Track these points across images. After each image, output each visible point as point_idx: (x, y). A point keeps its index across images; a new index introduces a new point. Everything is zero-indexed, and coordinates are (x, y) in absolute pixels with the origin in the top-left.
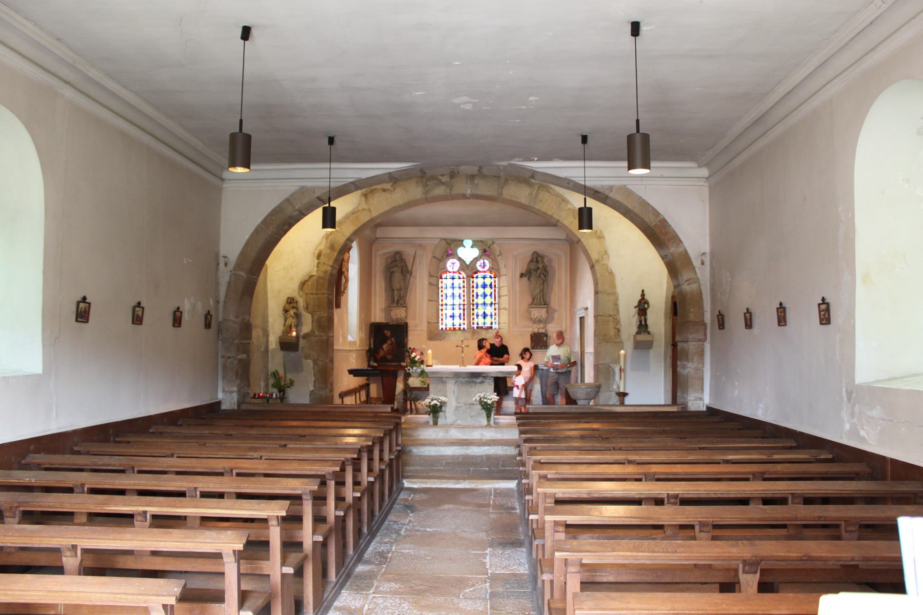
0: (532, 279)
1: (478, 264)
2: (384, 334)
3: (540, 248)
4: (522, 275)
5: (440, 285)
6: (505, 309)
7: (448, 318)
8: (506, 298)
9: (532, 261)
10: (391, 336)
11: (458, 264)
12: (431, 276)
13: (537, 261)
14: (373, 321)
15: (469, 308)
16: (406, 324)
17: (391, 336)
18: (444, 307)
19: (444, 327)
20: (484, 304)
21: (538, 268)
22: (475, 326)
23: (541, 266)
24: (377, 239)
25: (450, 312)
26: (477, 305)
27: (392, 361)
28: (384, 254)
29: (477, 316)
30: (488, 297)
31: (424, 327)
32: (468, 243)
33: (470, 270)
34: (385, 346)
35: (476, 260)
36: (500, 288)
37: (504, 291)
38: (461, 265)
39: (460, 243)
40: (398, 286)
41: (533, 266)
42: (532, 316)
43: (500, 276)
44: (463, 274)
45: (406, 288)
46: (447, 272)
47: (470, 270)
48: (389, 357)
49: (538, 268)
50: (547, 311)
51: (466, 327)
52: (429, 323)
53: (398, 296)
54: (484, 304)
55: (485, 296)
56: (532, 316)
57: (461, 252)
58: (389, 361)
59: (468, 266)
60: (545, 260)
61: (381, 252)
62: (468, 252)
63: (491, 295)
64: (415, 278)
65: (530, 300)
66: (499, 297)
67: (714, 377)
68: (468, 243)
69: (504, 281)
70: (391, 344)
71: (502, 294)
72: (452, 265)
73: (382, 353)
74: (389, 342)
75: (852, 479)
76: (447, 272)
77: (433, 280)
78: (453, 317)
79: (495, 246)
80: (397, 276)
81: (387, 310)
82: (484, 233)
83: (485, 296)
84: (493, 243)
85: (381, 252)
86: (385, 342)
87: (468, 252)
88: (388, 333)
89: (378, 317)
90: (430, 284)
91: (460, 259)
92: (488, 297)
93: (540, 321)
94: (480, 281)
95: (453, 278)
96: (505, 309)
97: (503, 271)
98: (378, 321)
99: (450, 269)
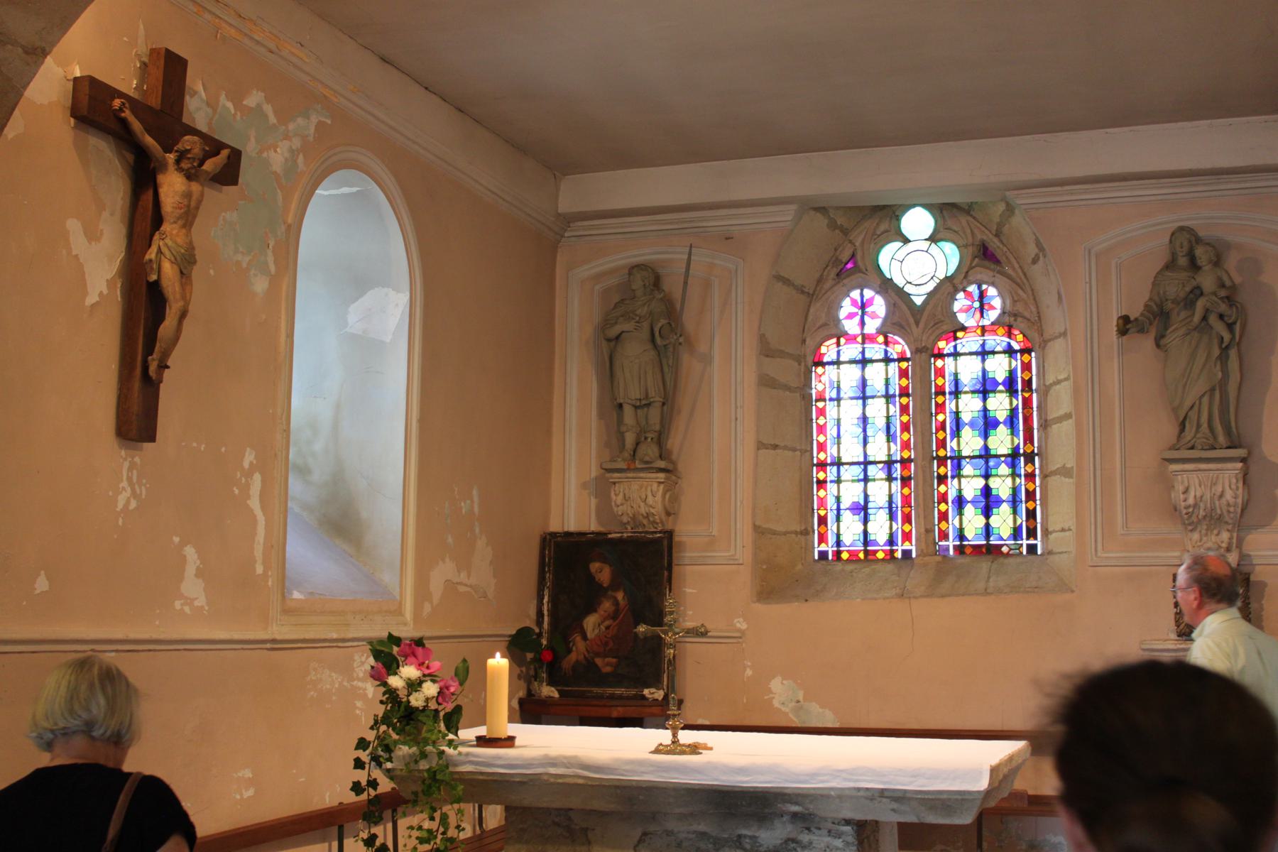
0: (1173, 338)
1: (960, 302)
2: (591, 578)
3: (1209, 214)
4: (1125, 326)
5: (816, 387)
6: (1065, 472)
7: (847, 516)
8: (1068, 426)
9: (1170, 265)
10: (615, 586)
11: (879, 306)
12: (767, 350)
13: (1194, 266)
14: (555, 527)
15: (923, 466)
16: (670, 534)
17: (615, 586)
18: (832, 472)
19: (829, 548)
20: (986, 455)
21: (1197, 292)
22: (951, 543)
23: (1207, 281)
24: (569, 220)
25: (851, 493)
26: (958, 460)
27: (616, 679)
28: (599, 277)
29: (960, 502)
30: (1002, 431)
31: (741, 546)
32: (918, 222)
33: (923, 326)
34: (591, 623)
35: (949, 287)
36: (1045, 391)
37: (1062, 400)
38: (892, 308)
39: (883, 219)
40: (635, 393)
41: (1175, 288)
42: (1177, 496)
43: (1044, 343)
44: (900, 346)
45: (668, 402)
46: (840, 335)
47: (923, 326)
48: (605, 665)
49: (1197, 292)
50: (1245, 477)
51: (912, 547)
52: (757, 529)
53: (645, 431)
54: (986, 455)
55: (988, 424)
56: (1177, 496)
57: (890, 259)
58: (603, 680)
59: (916, 312)
60: (1231, 262)
61: (585, 271)
62: (918, 258)
63: (1011, 421)
64: (707, 360)
65: (1168, 430)
66: (1044, 425)
67: (343, 195)
68: (918, 222)
69: (1059, 364)
70: (614, 616)
71: (1052, 415)
72: (863, 311)
73: (579, 649)
74: (607, 605)
75: (649, 214)
76: (840, 335)
77: (783, 370)
78: (862, 509)
79: (1017, 220)
80: (635, 353)
81: (601, 488)
82: (970, 167)
83: (988, 424)
84: (1010, 209)
85: (585, 271)
86: (591, 609)
87: (918, 258)
88: (602, 572)
89: (574, 512)
90: (766, 382)
91: (887, 287)
92: (1002, 431)
93: (1214, 520)
94: (969, 370)
95: (864, 362)
96: (1065, 472)
97: (1055, 319)
98: (572, 527)
99: (851, 327)
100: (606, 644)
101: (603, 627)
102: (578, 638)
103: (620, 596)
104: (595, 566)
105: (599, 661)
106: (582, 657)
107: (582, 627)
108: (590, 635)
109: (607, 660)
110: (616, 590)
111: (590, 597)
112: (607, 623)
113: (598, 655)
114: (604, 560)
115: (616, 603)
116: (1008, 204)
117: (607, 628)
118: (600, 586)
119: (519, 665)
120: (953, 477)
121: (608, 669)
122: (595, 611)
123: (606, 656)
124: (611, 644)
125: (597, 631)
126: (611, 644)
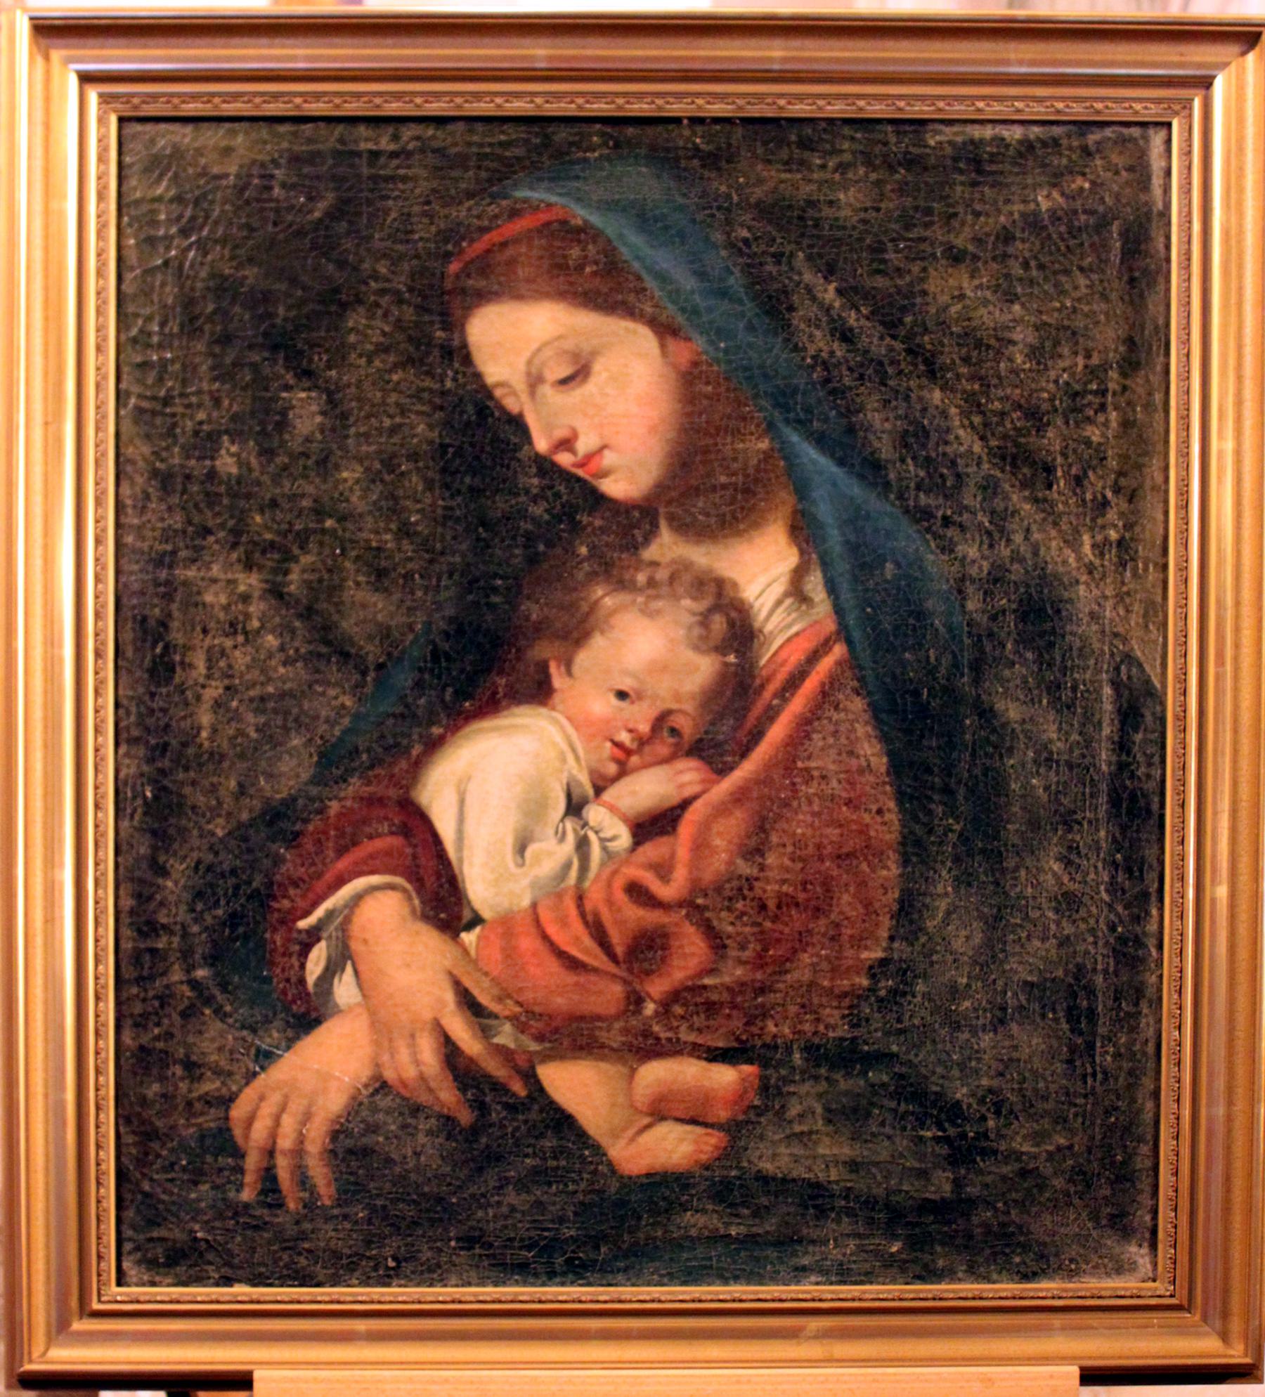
2: (482, 435)
10: (705, 488)
17: (705, 488)
34: (497, 789)
70: (720, 726)
74: (639, 650)
86: (485, 666)
88: (589, 383)
100: (647, 949)
101: (609, 824)
102: (380, 912)
103: (762, 568)
104: (513, 339)
105: (577, 1086)
106: (418, 1062)
107: (416, 824)
108: (487, 882)
109: (656, 1074)
110: (732, 516)
111: (496, 570)
112: (649, 788)
113: (574, 1036)
114: (604, 284)
115: (736, 631)
116: (377, 1091)
117: (653, 825)
118: (575, 496)
119: (732, 599)
120: (1105, 366)
121: (674, 1146)
122: (539, 691)
123: (648, 1047)
124: (690, 952)
125: (553, 852)
126: (690, 952)
